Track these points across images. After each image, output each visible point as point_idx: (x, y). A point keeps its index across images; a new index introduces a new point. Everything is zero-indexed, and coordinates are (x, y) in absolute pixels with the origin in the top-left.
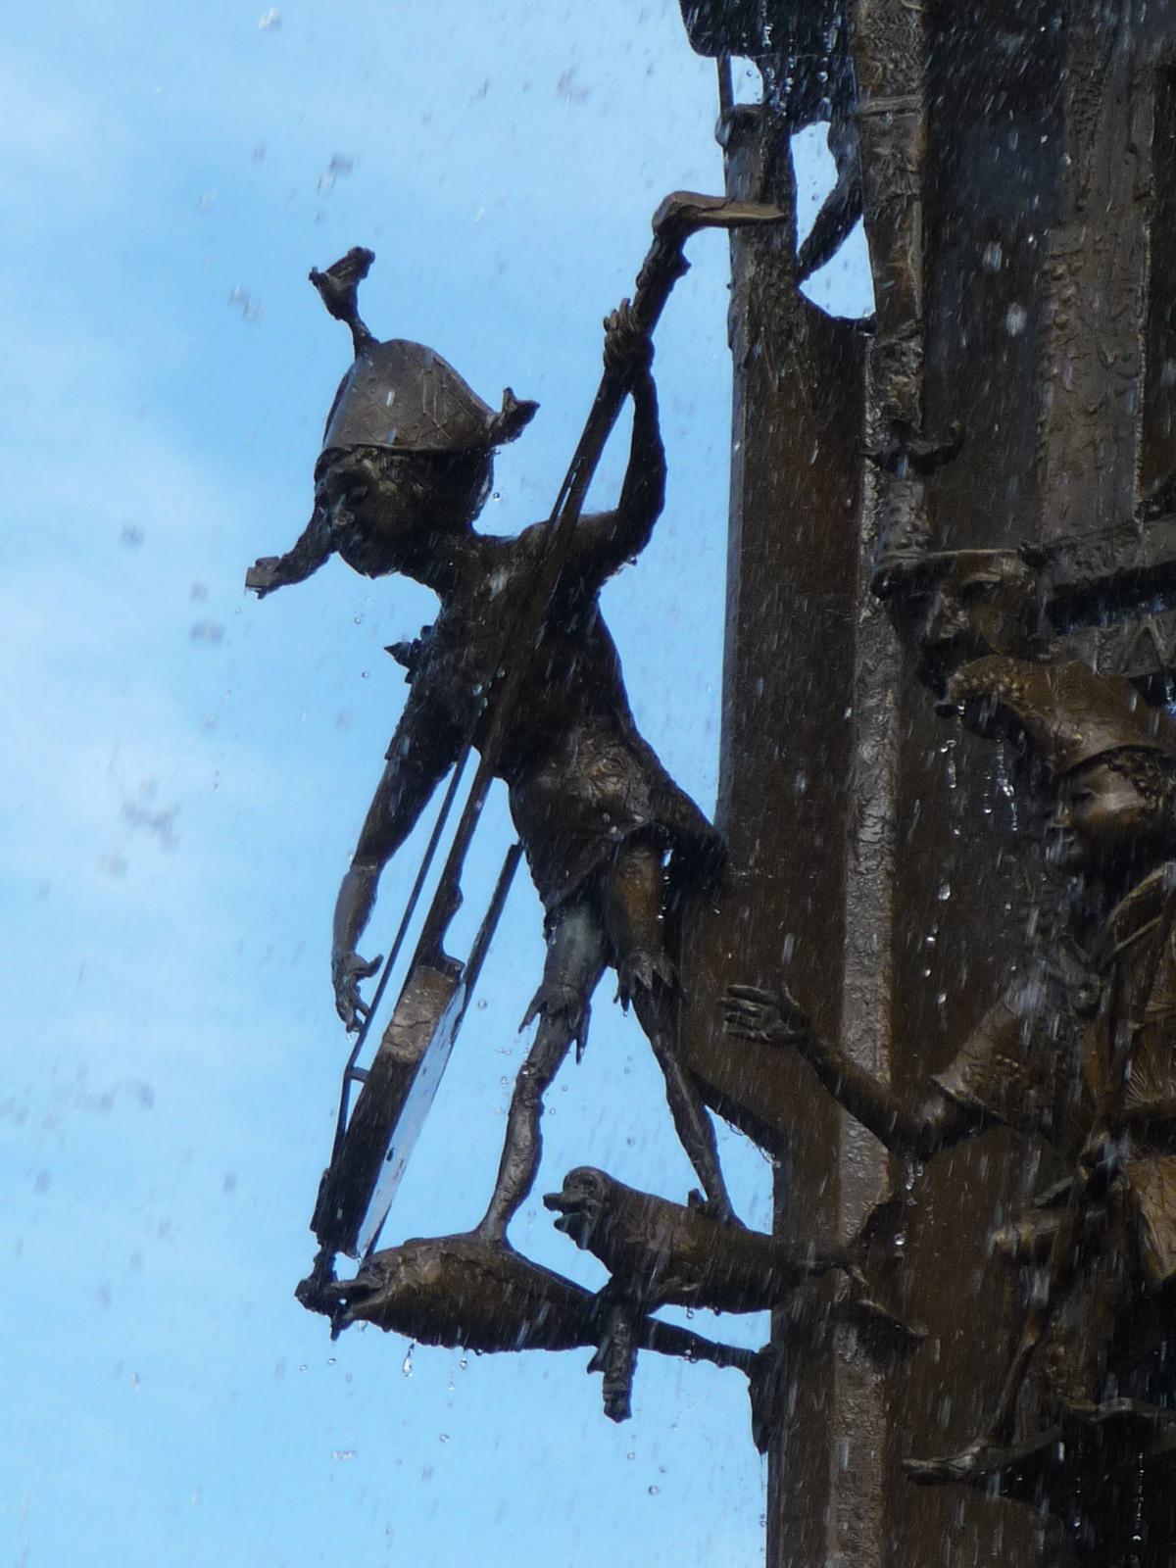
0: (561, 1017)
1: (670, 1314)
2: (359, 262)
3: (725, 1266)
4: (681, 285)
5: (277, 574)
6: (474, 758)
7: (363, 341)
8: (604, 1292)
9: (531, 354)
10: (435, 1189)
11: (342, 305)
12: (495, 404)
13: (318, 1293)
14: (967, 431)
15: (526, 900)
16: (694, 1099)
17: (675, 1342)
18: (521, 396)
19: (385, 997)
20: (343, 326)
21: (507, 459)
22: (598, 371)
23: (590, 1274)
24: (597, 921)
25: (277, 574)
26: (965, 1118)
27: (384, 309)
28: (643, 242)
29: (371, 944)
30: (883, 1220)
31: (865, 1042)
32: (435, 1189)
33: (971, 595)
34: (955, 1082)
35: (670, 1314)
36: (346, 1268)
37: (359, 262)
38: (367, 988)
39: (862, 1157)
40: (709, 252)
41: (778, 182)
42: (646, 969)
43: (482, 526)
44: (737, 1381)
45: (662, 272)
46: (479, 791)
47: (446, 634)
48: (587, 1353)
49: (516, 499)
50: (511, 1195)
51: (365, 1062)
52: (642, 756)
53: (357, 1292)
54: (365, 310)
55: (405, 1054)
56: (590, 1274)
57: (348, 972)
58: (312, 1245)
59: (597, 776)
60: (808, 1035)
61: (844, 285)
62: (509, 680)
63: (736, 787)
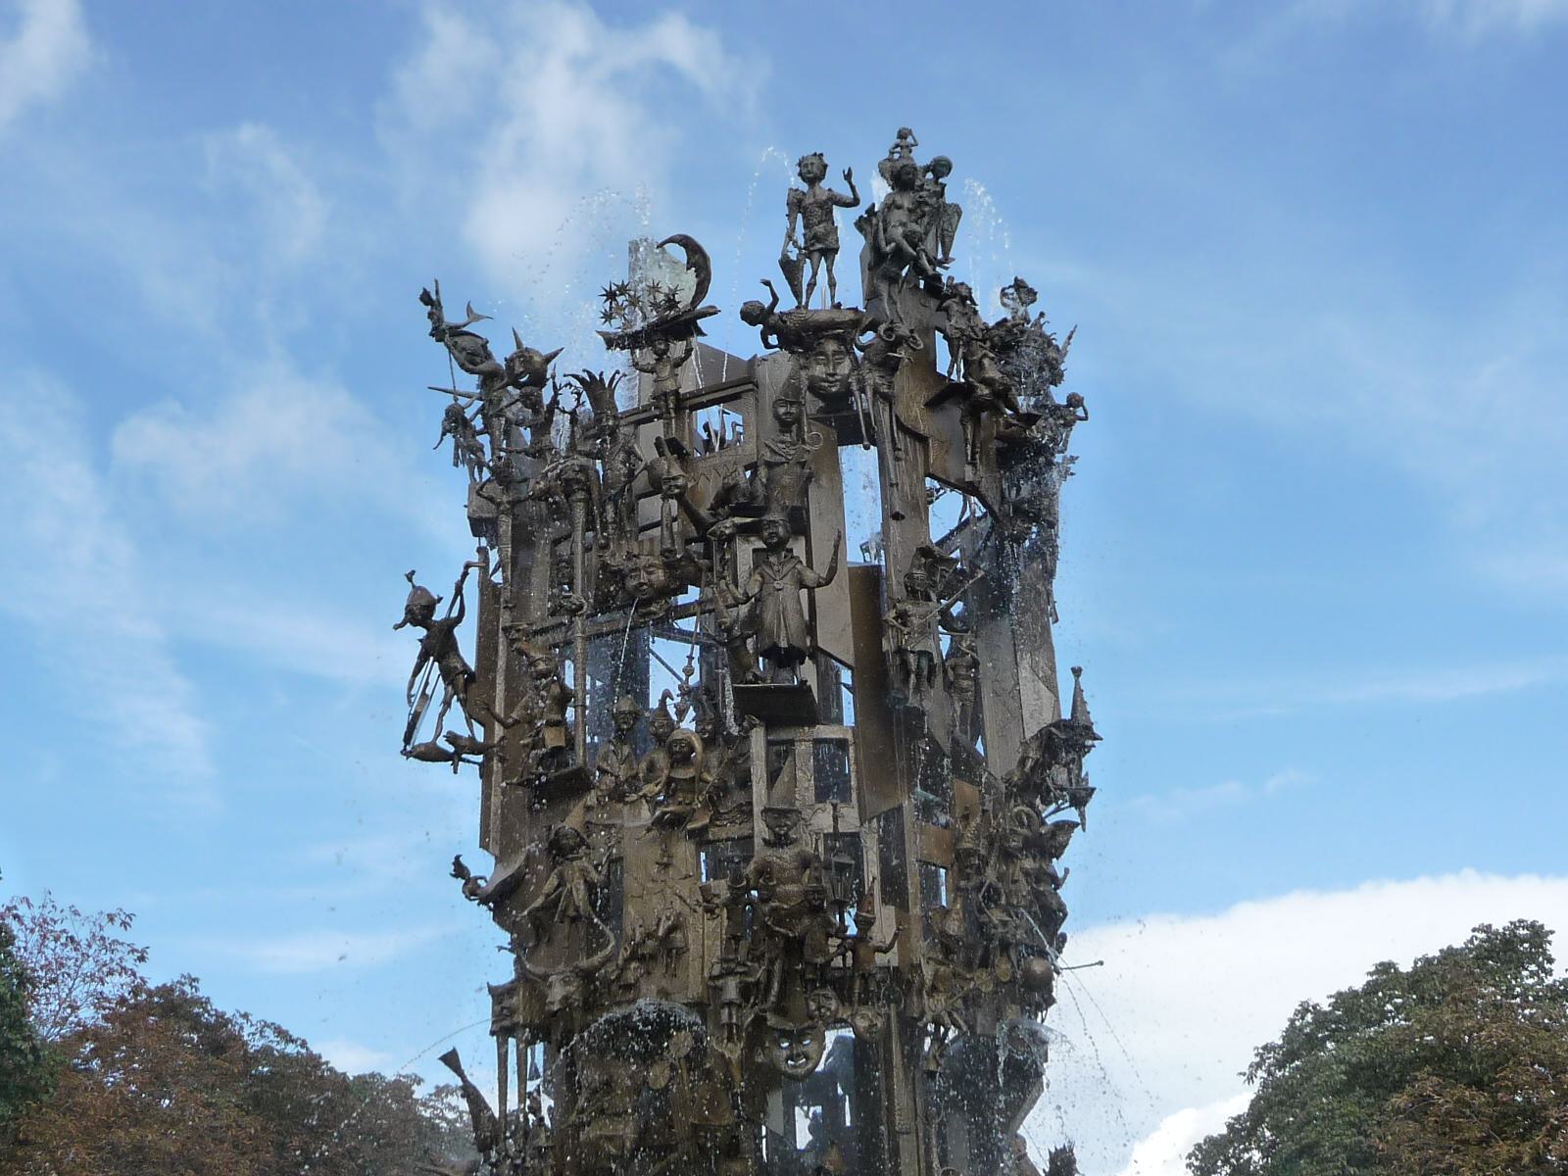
0: (447, 704)
1: (464, 756)
2: (413, 572)
3: (475, 748)
4: (468, 577)
5: (398, 627)
6: (432, 658)
7: (414, 586)
8: (456, 752)
9: (442, 588)
10: (424, 735)
11: (410, 580)
12: (436, 598)
13: (404, 752)
14: (518, 605)
15: (441, 684)
16: (469, 717)
17: (464, 760)
18: (441, 596)
19: (416, 700)
20: (410, 584)
21: (438, 606)
22: (454, 592)
23: (451, 749)
24: (453, 687)
25: (398, 627)
26: (516, 722)
27: (417, 581)
28: (462, 570)
29: (413, 692)
30: (502, 739)
31: (499, 708)
32: (424, 735)
33: (518, 631)
34: (514, 715)
35: (464, 756)
36: (409, 748)
37: (413, 572)
38: (413, 699)
39: (499, 731)
40: (474, 572)
41: (486, 560)
42: (461, 696)
43: (433, 618)
44: (477, 767)
45: (465, 574)
46: (432, 665)
47: (428, 637)
48: (451, 762)
49: (440, 614)
50: (437, 736)
51: (412, 712)
52: (462, 659)
53: (411, 752)
54: (414, 581)
55: (419, 710)
56: (451, 749)
57: (409, 696)
58: (403, 744)
59: (454, 663)
60: (489, 708)
61: (498, 578)
62: (439, 645)
63: (477, 667)
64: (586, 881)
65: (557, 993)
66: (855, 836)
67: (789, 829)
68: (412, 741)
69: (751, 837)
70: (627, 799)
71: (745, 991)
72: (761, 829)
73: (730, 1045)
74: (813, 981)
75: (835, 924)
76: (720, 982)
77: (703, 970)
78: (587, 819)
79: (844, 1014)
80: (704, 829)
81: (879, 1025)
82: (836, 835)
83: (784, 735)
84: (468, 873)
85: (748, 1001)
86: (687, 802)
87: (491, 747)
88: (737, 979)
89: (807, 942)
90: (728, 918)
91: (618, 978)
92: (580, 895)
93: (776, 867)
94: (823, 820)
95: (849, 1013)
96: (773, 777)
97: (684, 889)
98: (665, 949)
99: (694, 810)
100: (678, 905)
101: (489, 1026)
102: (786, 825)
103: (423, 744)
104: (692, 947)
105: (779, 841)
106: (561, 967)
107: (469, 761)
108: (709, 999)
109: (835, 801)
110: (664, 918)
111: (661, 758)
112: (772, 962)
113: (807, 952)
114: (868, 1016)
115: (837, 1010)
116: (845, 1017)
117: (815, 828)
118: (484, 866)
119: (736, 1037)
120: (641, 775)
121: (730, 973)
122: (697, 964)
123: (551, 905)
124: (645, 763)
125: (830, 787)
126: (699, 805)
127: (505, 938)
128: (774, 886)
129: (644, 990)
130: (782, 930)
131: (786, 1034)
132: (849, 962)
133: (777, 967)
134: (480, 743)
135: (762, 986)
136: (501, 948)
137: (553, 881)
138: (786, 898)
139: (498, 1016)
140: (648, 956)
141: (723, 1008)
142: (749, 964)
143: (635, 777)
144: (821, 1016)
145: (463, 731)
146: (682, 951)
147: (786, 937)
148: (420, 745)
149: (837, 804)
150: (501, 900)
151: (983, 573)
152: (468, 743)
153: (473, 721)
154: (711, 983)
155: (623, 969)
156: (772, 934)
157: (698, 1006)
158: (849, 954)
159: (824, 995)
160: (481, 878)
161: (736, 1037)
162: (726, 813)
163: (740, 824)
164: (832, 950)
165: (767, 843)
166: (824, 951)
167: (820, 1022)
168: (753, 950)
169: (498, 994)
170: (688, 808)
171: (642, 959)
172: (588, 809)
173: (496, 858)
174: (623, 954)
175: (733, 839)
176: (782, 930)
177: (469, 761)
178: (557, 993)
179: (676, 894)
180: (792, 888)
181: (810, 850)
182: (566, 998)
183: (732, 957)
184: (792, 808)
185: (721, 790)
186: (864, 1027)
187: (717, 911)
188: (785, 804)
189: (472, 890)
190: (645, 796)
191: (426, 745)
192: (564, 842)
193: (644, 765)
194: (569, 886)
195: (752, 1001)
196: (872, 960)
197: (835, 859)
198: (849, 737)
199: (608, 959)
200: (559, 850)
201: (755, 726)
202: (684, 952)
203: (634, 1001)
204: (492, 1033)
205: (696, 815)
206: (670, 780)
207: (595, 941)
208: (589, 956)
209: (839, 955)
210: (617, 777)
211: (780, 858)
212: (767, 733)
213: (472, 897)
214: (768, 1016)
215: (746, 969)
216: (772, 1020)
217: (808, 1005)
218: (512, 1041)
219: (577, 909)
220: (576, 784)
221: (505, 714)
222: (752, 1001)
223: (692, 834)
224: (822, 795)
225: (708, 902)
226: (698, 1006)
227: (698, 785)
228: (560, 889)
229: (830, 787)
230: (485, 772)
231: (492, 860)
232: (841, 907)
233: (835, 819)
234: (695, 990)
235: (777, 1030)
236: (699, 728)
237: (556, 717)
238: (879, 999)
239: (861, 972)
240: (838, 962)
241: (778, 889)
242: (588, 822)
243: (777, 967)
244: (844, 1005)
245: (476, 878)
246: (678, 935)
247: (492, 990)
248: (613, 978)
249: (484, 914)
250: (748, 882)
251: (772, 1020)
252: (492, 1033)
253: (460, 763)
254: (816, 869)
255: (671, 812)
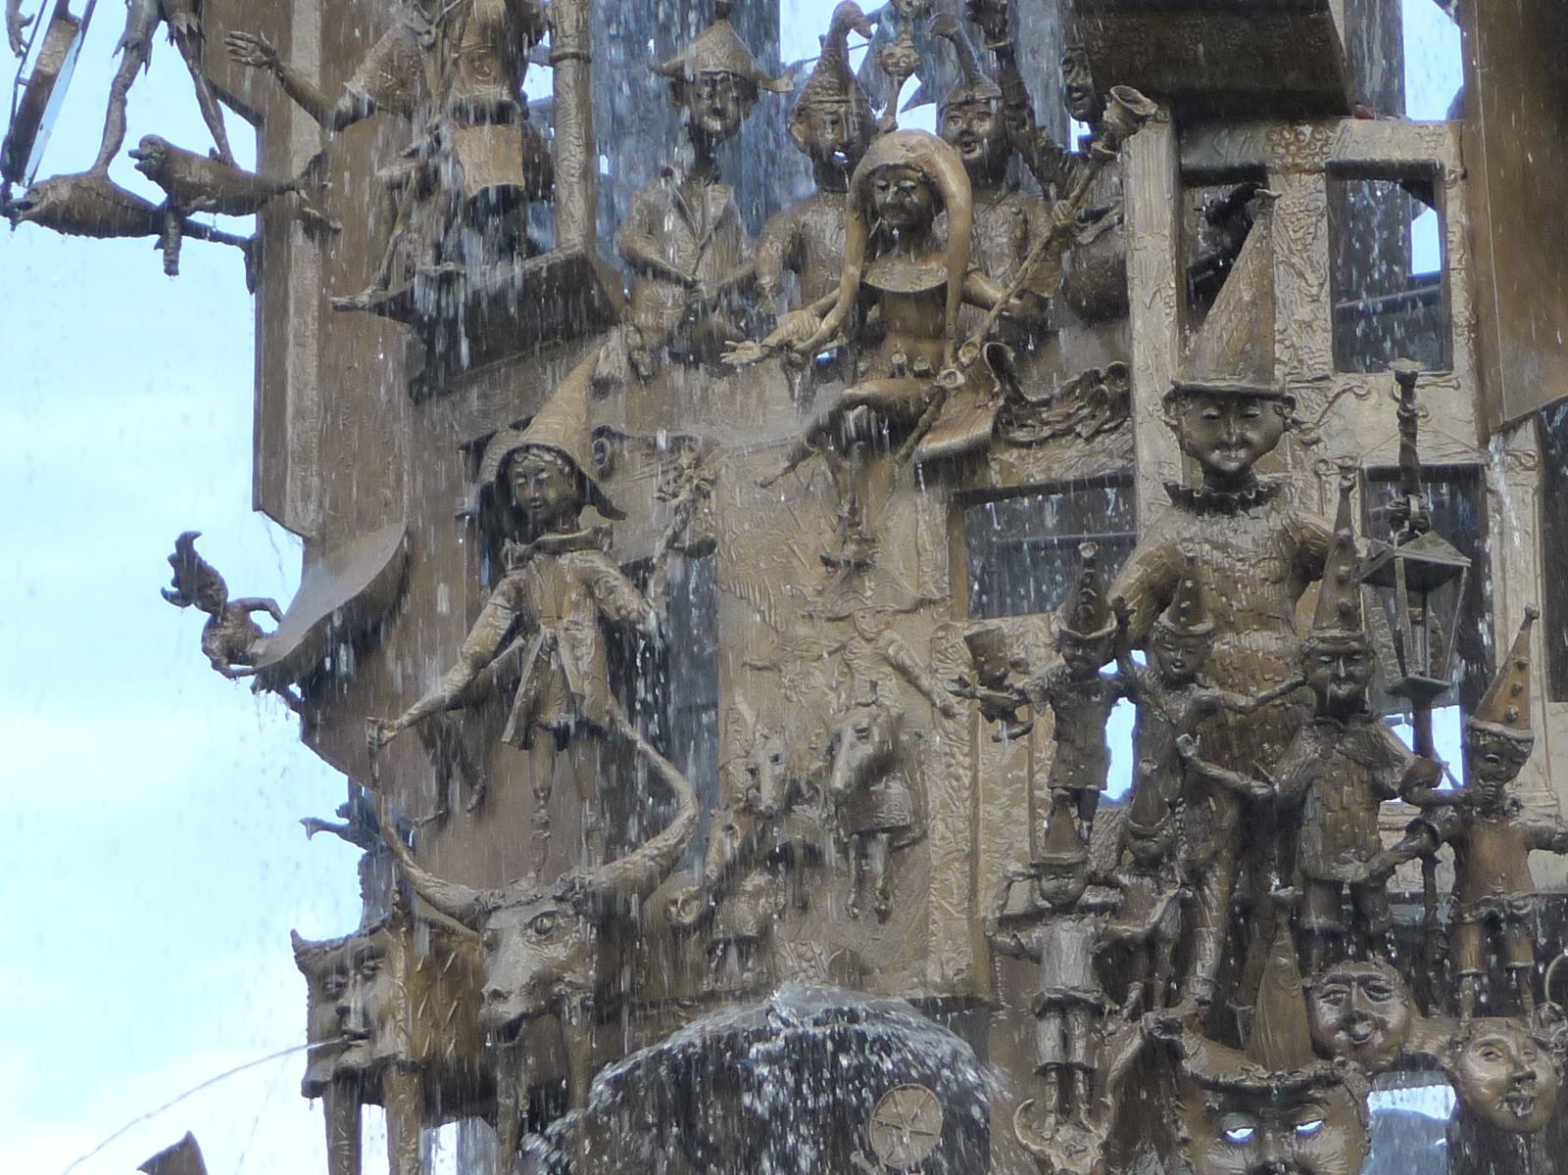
0: (136, 50)
1: (199, 218)
3: (237, 196)
8: (171, 204)
16: (213, 95)
17: (198, 232)
19: (37, 39)
23: (154, 194)
31: (305, 61)
35: (199, 218)
38: (26, 33)
44: (237, 254)
51: (27, 75)
53: (26, 206)
55: (50, 70)
56: (154, 194)
64: (602, 619)
65: (514, 966)
66: (1467, 479)
67: (1257, 455)
68: (28, 172)
69: (1125, 482)
70: (728, 358)
71: (1116, 963)
72: (1157, 452)
73: (1066, 1133)
74: (1331, 935)
75: (1401, 759)
76: (1033, 936)
77: (973, 895)
78: (598, 422)
79: (1429, 1040)
80: (975, 455)
81: (1542, 1077)
82: (1408, 475)
83: (1234, 149)
84: (222, 588)
85: (1120, 997)
86: (919, 366)
87: (282, 190)
88: (1089, 925)
89: (1309, 812)
90: (1059, 736)
91: (706, 920)
92: (580, 658)
93: (1211, 577)
94: (1362, 422)
95: (1444, 1039)
96: (1200, 288)
97: (909, 641)
98: (865, 820)
99: (941, 395)
100: (891, 689)
101: (298, 1066)
102: (1245, 443)
103: (65, 178)
104: (938, 828)
105: (1223, 493)
106: (526, 886)
107: (217, 237)
108: (993, 985)
109: (1406, 366)
110: (849, 736)
111: (834, 230)
112: (1196, 877)
113: (1311, 843)
114: (1505, 1049)
115: (1406, 1029)
116: (1430, 1049)
117: (1333, 448)
118: (264, 565)
119: (1083, 1107)
120: (766, 281)
121: (1067, 907)
122: (956, 875)
123: (481, 698)
124: (778, 245)
125: (1385, 322)
126: (961, 379)
127: (329, 789)
128: (1208, 635)
129: (787, 955)
130: (1232, 776)
131: (1243, 1101)
132: (1446, 878)
133: (1215, 890)
134: (248, 175)
135: (1166, 951)
136: (315, 826)
137: (496, 616)
138: (1246, 670)
139: (331, 1034)
140: (799, 853)
141: (1041, 1015)
142: (1124, 879)
143: (749, 287)
144: (1358, 1046)
145: (192, 137)
146: (903, 839)
147: (1242, 797)
148: (55, 181)
149: (1414, 375)
150: (326, 678)
151: (1044, 882)
152: (208, 177)
153: (222, 105)
154: (1004, 939)
155: (723, 888)
156: (1200, 789)
157: (959, 1009)
158: (1446, 853)
159: (1363, 982)
160: (261, 606)
161: (1083, 1107)
162: (1046, 403)
163: (1089, 440)
164: (1391, 840)
165: (1182, 498)
166: (1361, 844)
167: (1352, 1065)
168: (1138, 836)
169: (325, 970)
170: (924, 387)
171: (783, 859)
172: (601, 387)
173: (307, 541)
174: (725, 846)
175: (1064, 487)
176: (1232, 776)
177: (217, 237)
178: (514, 966)
179: (886, 659)
180: (1262, 641)
181: (1324, 521)
182: (542, 984)
183: (1069, 856)
184: (1262, 387)
185: (1028, 330)
186: (1493, 1084)
187: (1021, 713)
188: (1242, 374)
189: (231, 646)
190: (786, 346)
191: (76, 182)
192: (531, 491)
193: (773, 249)
194: (546, 631)
195: (1133, 995)
196: (1516, 874)
197: (1405, 552)
198: (1445, 154)
199: (671, 864)
200: (511, 519)
201: (1141, 120)
202: (914, 842)
203: (759, 990)
204: (312, 1089)
205: (952, 408)
206: (867, 295)
207: (627, 801)
208: (615, 843)
209: (1412, 854)
210: (690, 287)
211: (1223, 547)
212: (1179, 151)
213: (234, 667)
214: (1189, 1042)
215: (1113, 896)
216: (1199, 1057)
217: (1311, 1009)
218: (373, 1119)
219: (572, 701)
220: (568, 308)
221: (324, 80)
222: (1133, 995)
223: (937, 468)
224: (1355, 346)
225: (996, 683)
226: (959, 1009)
227: (955, 313)
228: (519, 641)
229: (1385, 322)
230: (264, 264)
231: (293, 549)
232: (1421, 698)
233: (1408, 423)
234: (949, 961)
235: (1215, 1087)
236: (955, 128)
237: (495, 93)
238: (1539, 999)
239: (1484, 911)
240: (1408, 877)
241: (1217, 646)
242: (601, 432)
243: (1215, 890)
244: (1425, 1013)
245: (248, 607)
246: (894, 789)
247: (307, 956)
248: (688, 919)
249: (275, 721)
250: (1123, 621)
251: (1199, 1057)
252: (312, 1089)
253: (186, 240)
254: (1342, 582)
255: (870, 402)
